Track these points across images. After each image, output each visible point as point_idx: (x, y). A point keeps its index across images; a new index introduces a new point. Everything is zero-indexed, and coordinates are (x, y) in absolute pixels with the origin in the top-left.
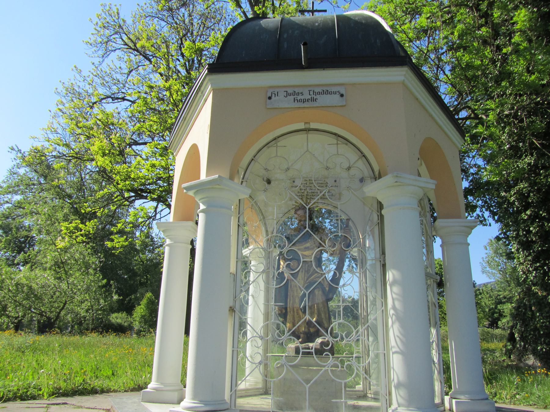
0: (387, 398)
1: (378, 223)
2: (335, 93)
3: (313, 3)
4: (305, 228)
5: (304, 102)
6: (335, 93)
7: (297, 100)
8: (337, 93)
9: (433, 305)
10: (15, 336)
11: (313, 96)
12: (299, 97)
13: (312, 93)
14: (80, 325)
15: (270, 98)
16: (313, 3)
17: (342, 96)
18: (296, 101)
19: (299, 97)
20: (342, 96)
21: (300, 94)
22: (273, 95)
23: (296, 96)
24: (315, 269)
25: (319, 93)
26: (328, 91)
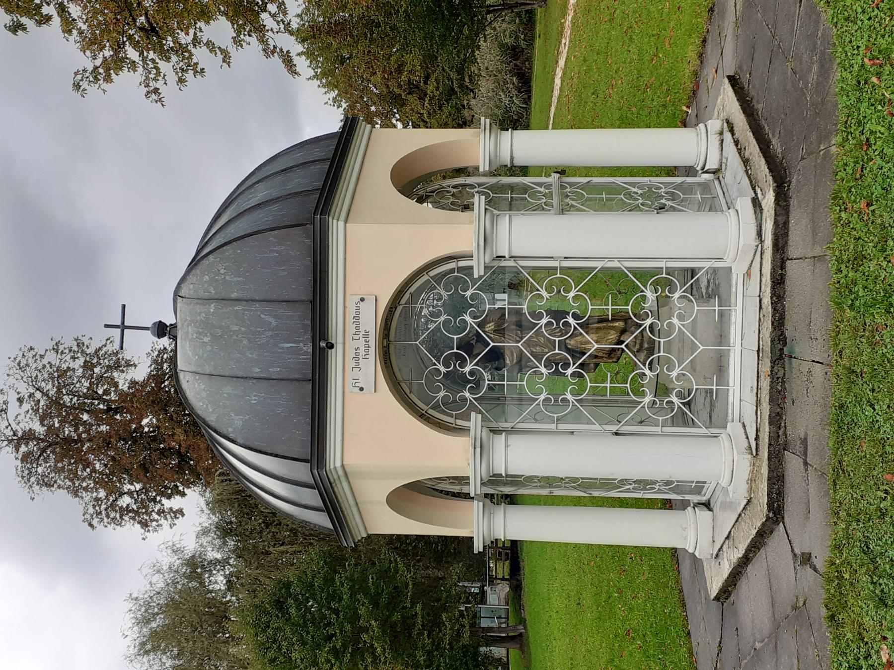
0: (607, 260)
1: (618, 261)
2: (358, 308)
3: (107, 326)
4: (518, 346)
5: (369, 347)
6: (358, 308)
7: (365, 355)
8: (358, 305)
9: (662, 206)
10: (275, 594)
11: (361, 336)
12: (362, 352)
13: (356, 337)
14: (95, 499)
15: (362, 389)
16: (107, 326)
17: (362, 300)
18: (367, 356)
19: (362, 352)
20: (362, 300)
21: (358, 351)
22: (357, 385)
23: (360, 357)
24: (650, 338)
25: (357, 328)
26: (354, 317)
